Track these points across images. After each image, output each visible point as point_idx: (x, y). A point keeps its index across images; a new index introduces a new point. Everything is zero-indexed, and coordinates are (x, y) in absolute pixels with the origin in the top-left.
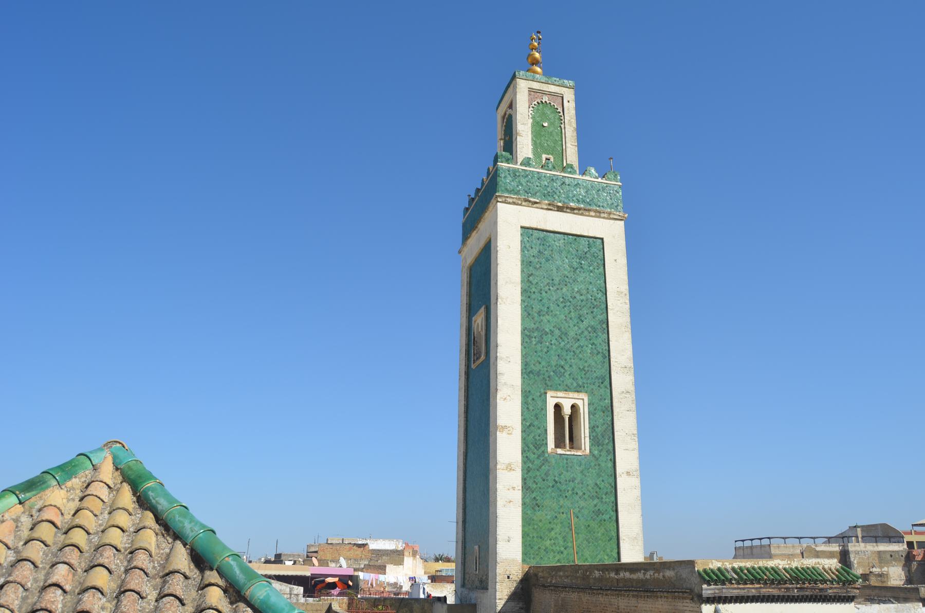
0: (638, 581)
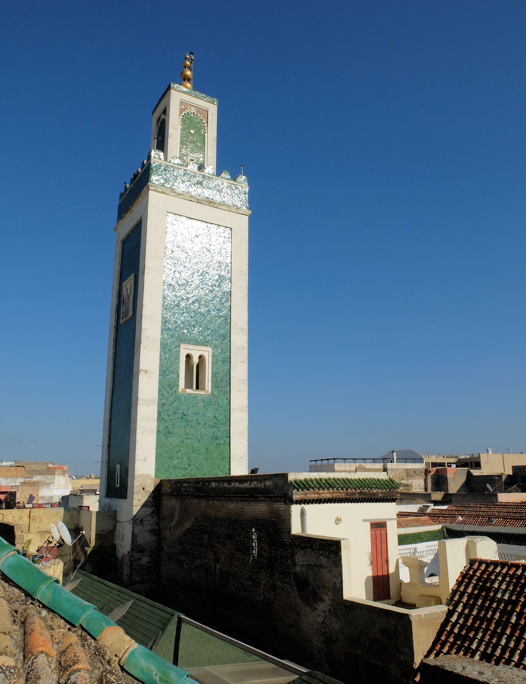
0: (247, 489)
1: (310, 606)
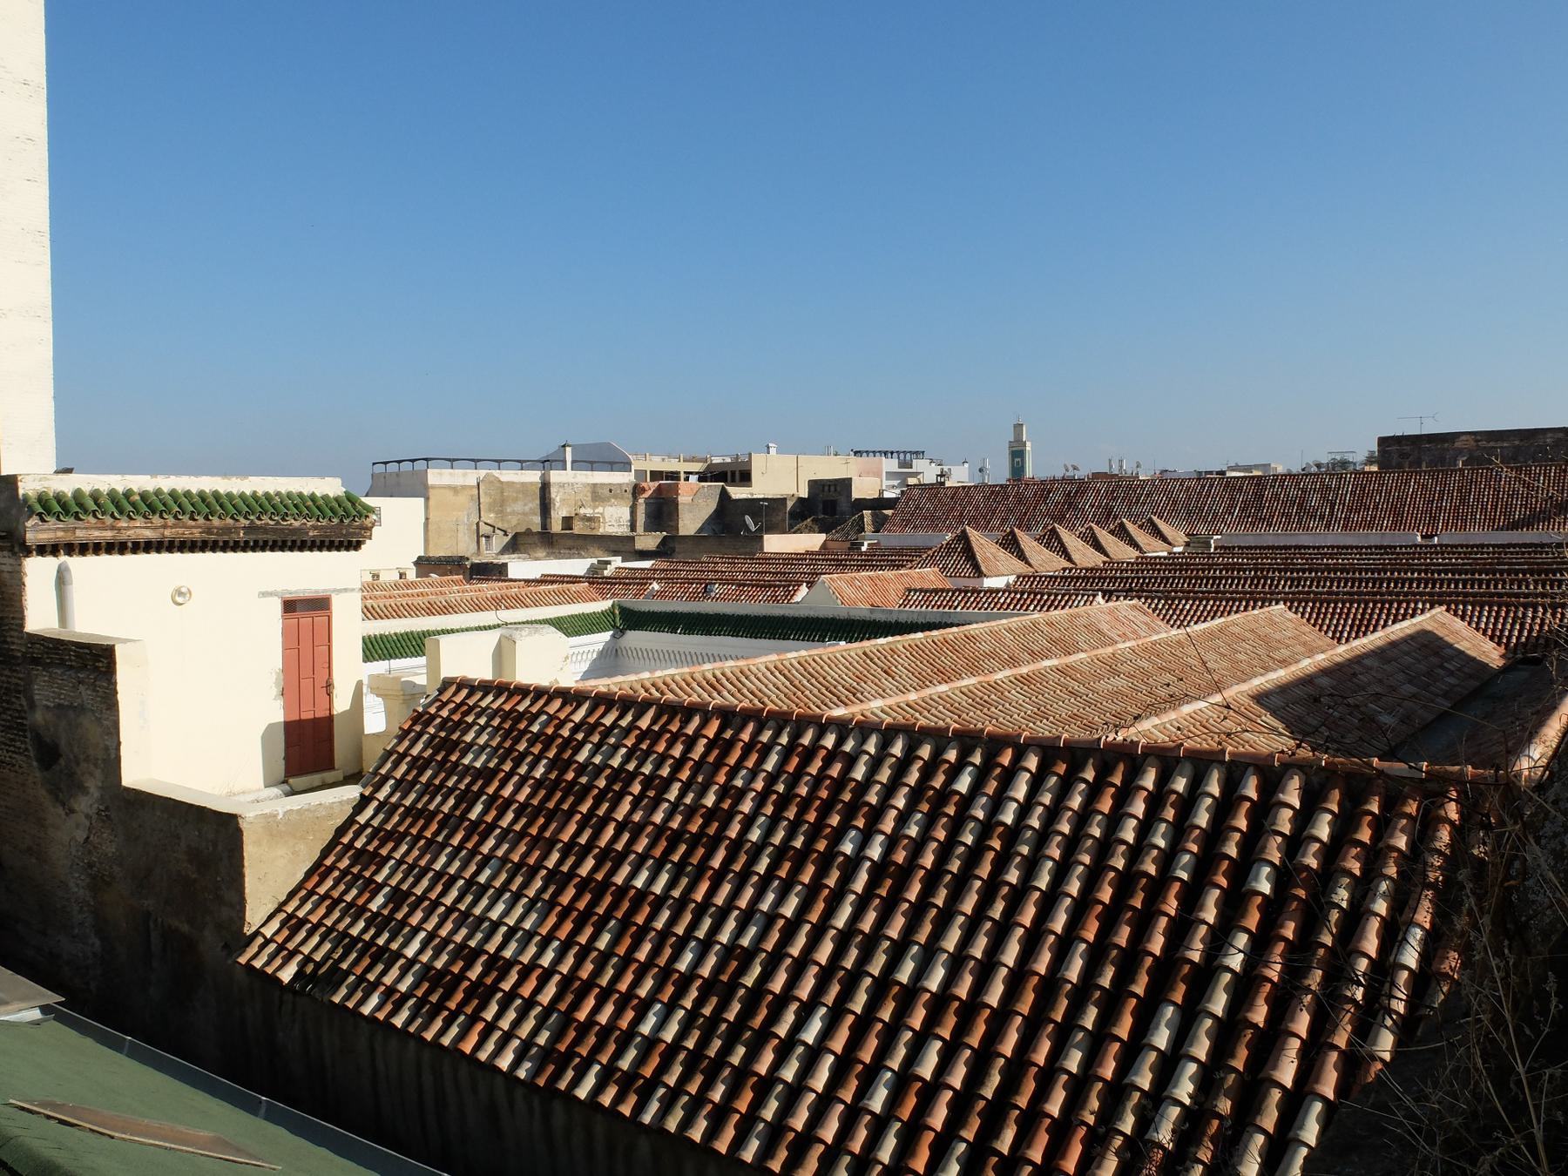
1: (63, 804)
